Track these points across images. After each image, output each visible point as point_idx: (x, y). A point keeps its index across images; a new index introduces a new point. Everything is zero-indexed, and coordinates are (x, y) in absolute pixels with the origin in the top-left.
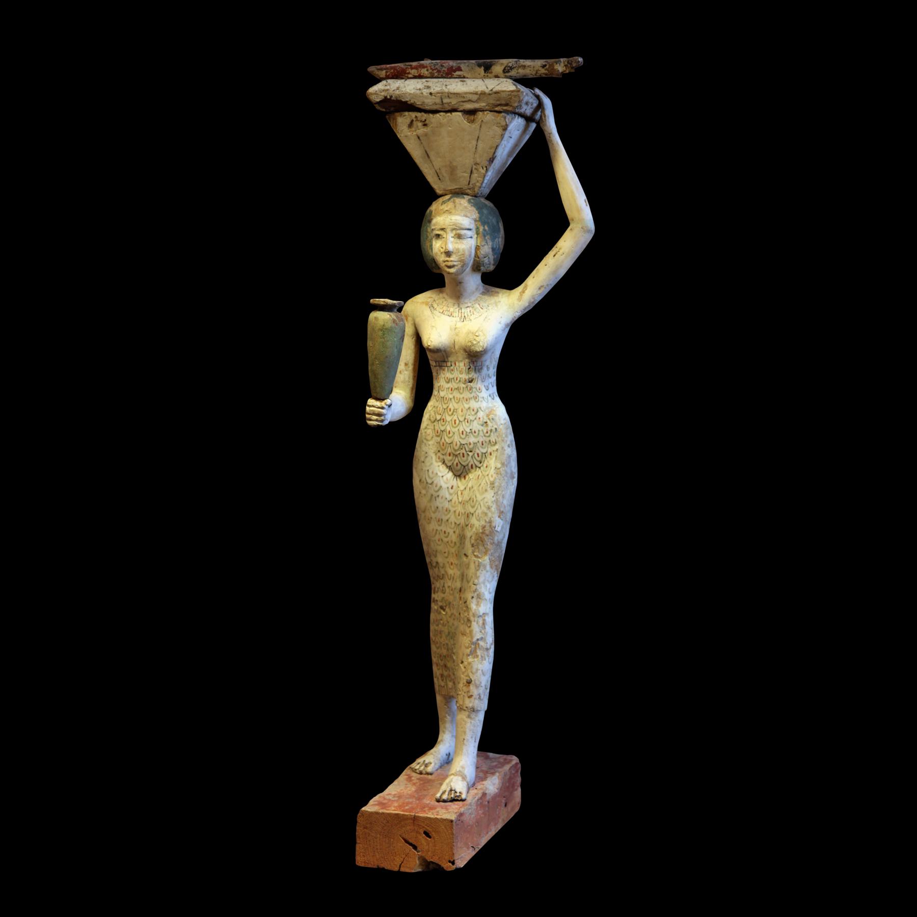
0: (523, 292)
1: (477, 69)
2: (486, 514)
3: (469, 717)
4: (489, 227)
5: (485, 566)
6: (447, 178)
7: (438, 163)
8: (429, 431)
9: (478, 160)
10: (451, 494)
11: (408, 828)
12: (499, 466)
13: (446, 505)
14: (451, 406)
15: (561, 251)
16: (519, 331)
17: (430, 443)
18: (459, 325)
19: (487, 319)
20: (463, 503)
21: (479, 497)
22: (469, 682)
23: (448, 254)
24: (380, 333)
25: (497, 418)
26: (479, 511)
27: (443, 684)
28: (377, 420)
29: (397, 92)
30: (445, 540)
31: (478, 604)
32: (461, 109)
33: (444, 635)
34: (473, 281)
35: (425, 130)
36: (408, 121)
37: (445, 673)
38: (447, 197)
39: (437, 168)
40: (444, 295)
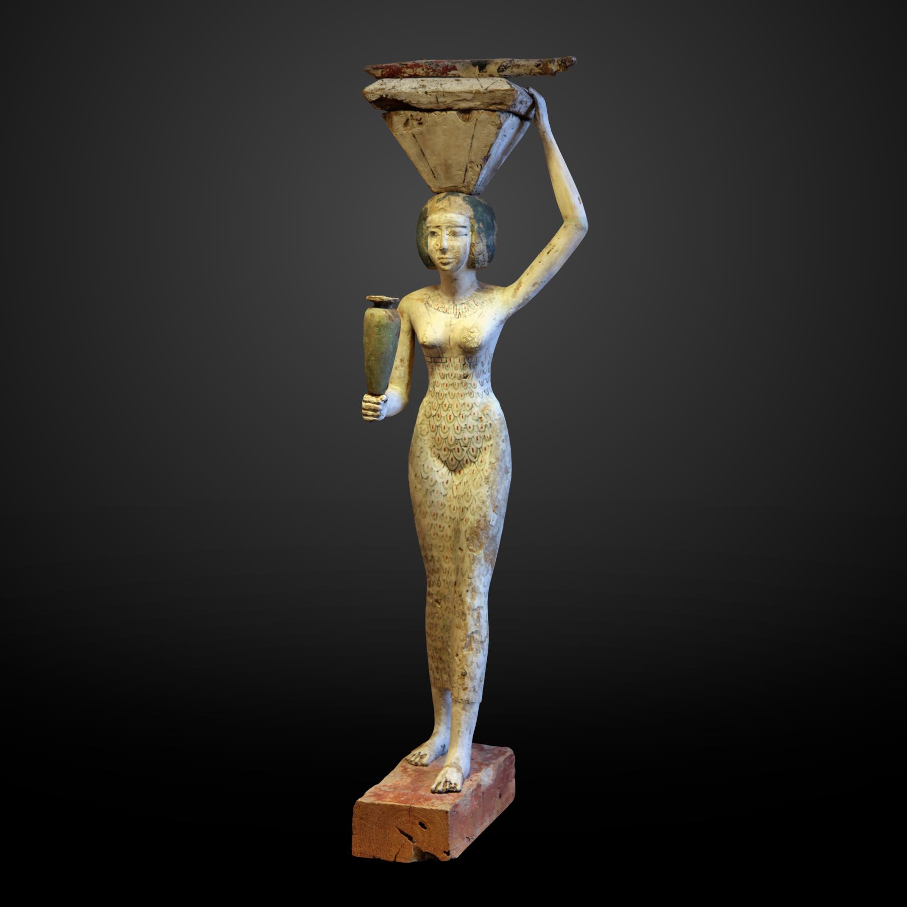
0: (518, 289)
1: (472, 68)
2: (481, 509)
3: (464, 709)
4: (483, 224)
5: (479, 560)
6: (442, 176)
7: (433, 161)
8: (424, 427)
9: (473, 159)
10: (446, 489)
11: (404, 819)
12: (494, 460)
13: (442, 499)
14: (446, 402)
15: (555, 249)
16: (513, 326)
17: (426, 438)
18: (454, 321)
19: (481, 316)
20: (458, 498)
21: (474, 492)
22: (464, 675)
23: (443, 251)
24: (376, 329)
25: (491, 414)
26: (474, 506)
27: (438, 676)
28: (372, 416)
29: (393, 91)
30: (440, 534)
31: (473, 598)
32: (456, 107)
33: (439, 629)
34: (467, 278)
35: (420, 128)
36: (404, 120)
37: (441, 666)
38: (442, 195)
39: (432, 166)
40: (440, 292)
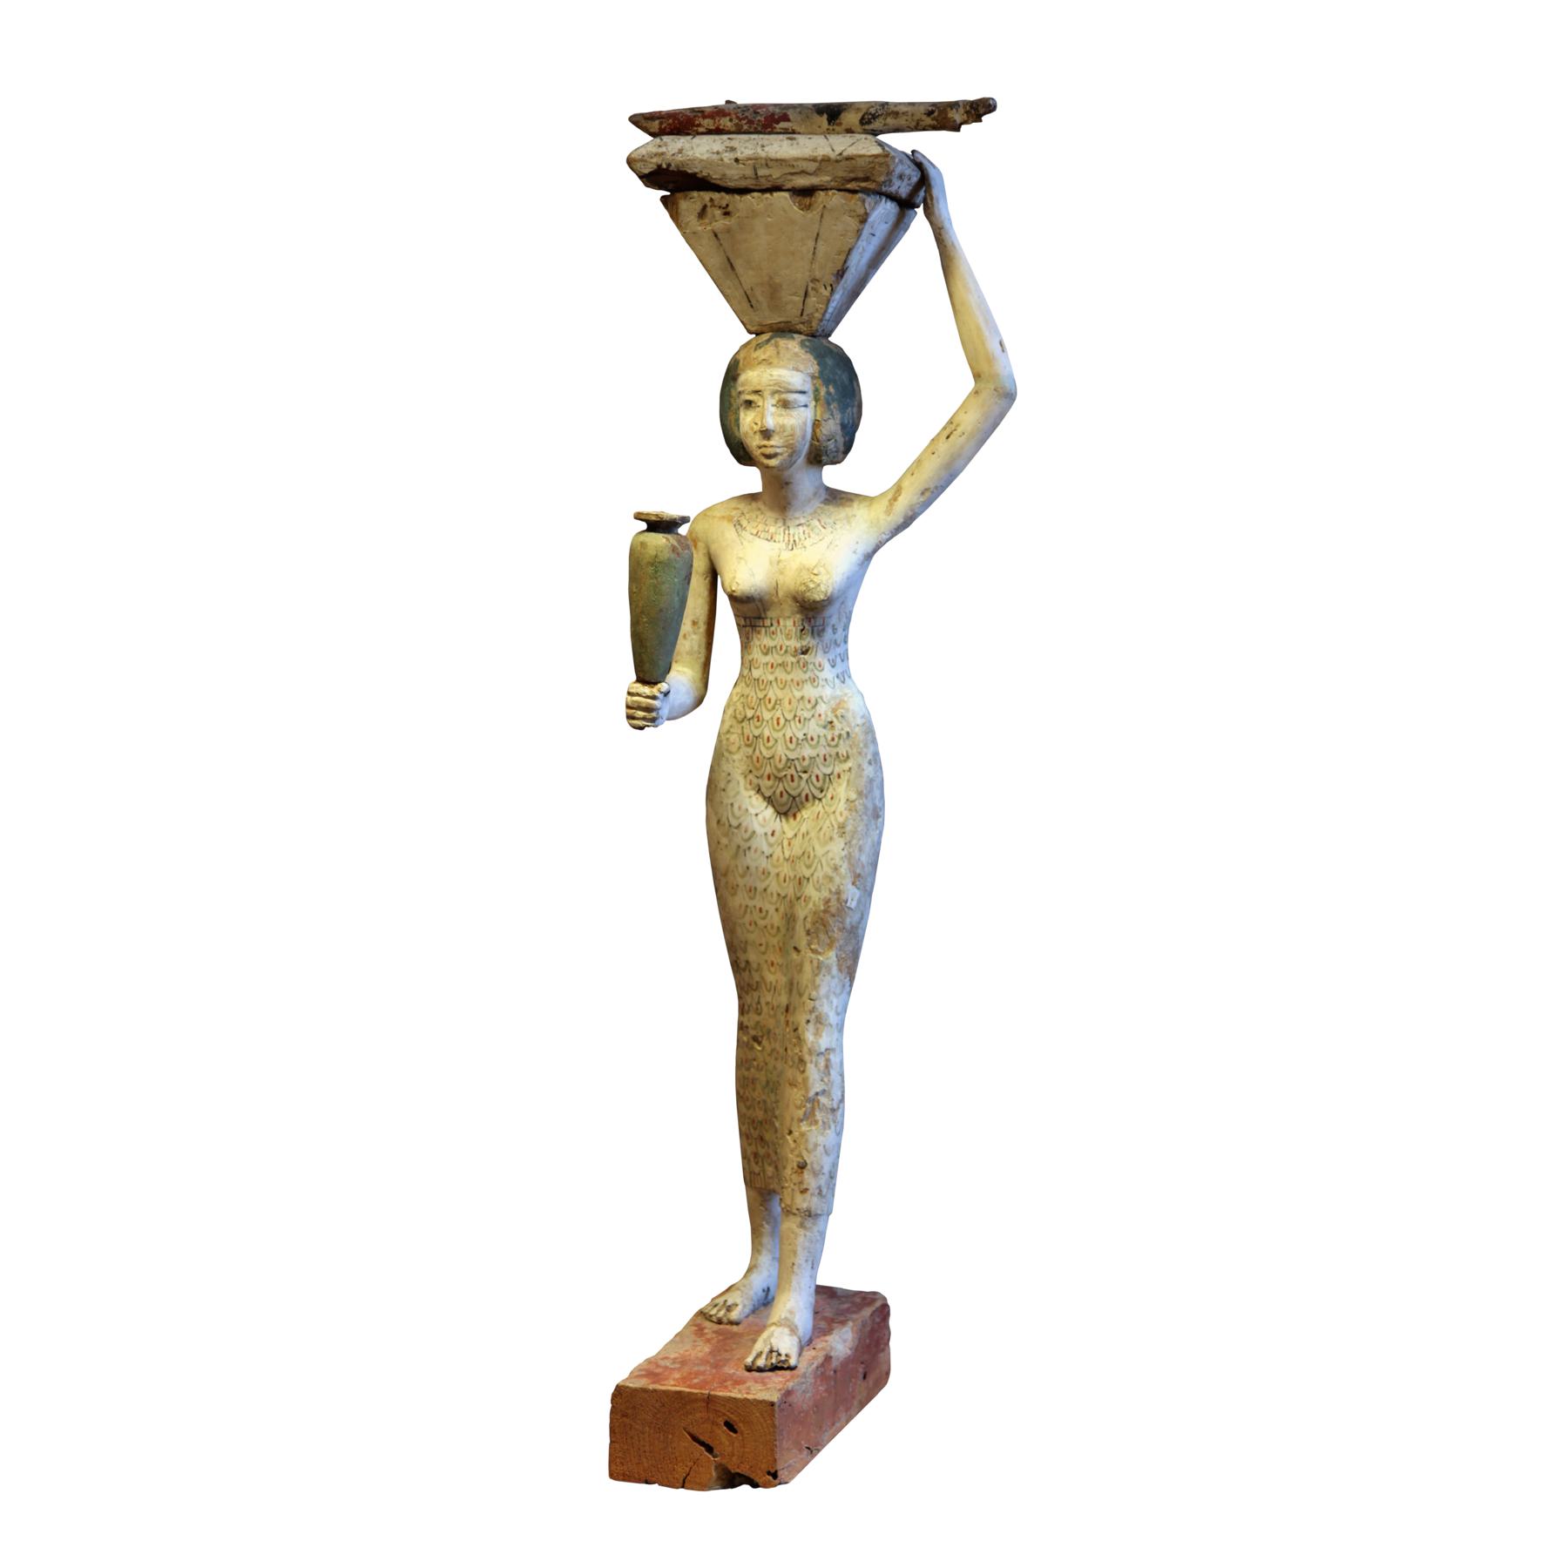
0: (895, 499)
2: (831, 879)
3: (802, 1225)
4: (836, 387)
5: (829, 969)
6: (765, 305)
8: (733, 738)
9: (818, 274)
10: (771, 845)
11: (698, 1415)
12: (853, 796)
13: (763, 863)
14: (771, 695)
15: (960, 430)
17: (736, 757)
18: (786, 555)
20: (791, 860)
21: (820, 851)
22: (802, 1167)
23: (766, 434)
24: (651, 570)
25: (849, 715)
26: (819, 874)
27: (757, 1169)
29: (679, 158)
30: (761, 923)
31: (817, 1034)
32: (789, 186)
33: (758, 1087)
35: (726, 222)
36: (698, 207)
37: (762, 1151)
39: (747, 287)
